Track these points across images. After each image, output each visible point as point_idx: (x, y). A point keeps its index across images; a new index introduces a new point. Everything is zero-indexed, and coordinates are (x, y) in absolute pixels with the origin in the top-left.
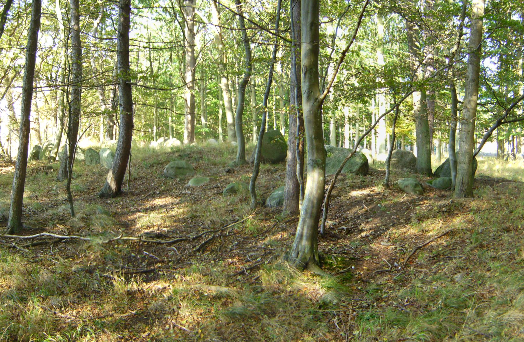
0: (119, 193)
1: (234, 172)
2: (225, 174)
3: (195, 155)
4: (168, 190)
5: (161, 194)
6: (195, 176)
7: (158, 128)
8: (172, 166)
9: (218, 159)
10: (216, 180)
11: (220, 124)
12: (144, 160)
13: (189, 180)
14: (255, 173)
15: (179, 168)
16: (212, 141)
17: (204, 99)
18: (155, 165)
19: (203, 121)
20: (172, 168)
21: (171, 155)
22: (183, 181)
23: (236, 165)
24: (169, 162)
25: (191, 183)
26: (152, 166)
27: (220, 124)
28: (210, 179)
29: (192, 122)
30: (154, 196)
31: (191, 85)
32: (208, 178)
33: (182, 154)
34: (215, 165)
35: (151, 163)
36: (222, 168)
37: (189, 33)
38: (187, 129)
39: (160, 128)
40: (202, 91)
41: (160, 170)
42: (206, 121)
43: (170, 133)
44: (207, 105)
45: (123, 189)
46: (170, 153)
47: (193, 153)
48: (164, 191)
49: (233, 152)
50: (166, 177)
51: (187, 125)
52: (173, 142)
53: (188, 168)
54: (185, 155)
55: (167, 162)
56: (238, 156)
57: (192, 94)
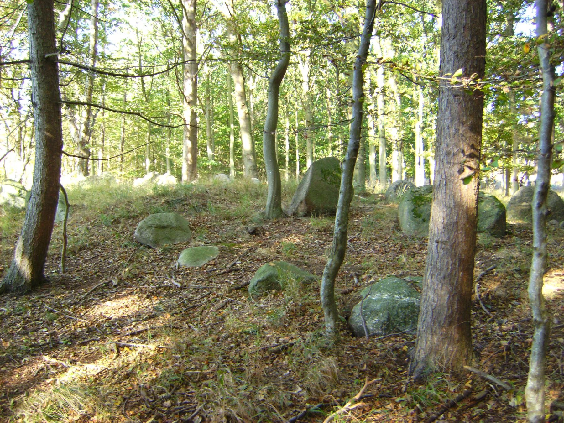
0: (39, 282)
1: (264, 234)
2: (247, 236)
3: (193, 202)
4: (136, 276)
5: (122, 287)
6: (193, 243)
7: (152, 161)
8: (150, 223)
9: (233, 208)
10: (233, 252)
11: (231, 155)
12: (105, 211)
13: (180, 250)
14: (336, 258)
15: (163, 227)
16: (221, 176)
17: (210, 124)
18: (122, 220)
19: (209, 152)
20: (149, 227)
21: (153, 201)
22: (169, 254)
23: (266, 220)
24: (147, 214)
25: (183, 259)
26: (116, 222)
27: (231, 155)
28: (221, 249)
29: (194, 150)
30: (103, 293)
31: (191, 99)
32: (216, 248)
33: (171, 199)
34: (228, 218)
35: (116, 216)
36: (242, 226)
37: (188, 25)
38: (187, 160)
39: (156, 161)
40: (207, 114)
41: (131, 229)
42: (213, 151)
43: (168, 167)
44: (214, 133)
45: (50, 272)
46: (153, 197)
47: (191, 197)
48: (127, 279)
49: (258, 195)
50: (139, 244)
51: (186, 155)
52: (167, 180)
53: (179, 228)
54: (178, 202)
55: (145, 213)
56: (268, 202)
57: (192, 112)
